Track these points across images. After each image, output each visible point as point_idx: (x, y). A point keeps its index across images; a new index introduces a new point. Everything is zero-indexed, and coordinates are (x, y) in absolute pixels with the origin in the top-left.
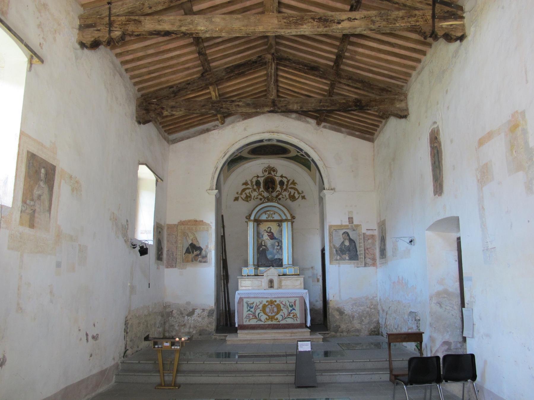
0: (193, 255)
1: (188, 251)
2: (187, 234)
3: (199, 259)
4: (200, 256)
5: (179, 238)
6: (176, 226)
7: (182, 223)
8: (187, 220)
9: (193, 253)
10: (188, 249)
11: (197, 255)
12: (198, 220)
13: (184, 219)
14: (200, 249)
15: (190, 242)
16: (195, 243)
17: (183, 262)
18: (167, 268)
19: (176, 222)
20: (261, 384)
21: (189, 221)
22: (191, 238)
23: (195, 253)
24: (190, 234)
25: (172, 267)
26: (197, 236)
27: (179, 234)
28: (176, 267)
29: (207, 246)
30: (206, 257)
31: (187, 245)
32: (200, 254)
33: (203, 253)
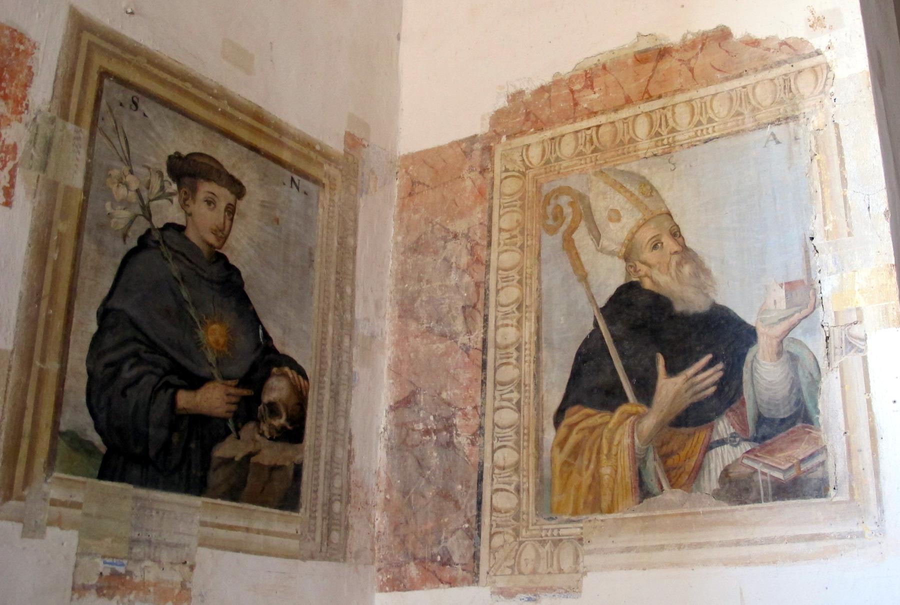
0: (649, 423)
1: (592, 384)
2: (581, 202)
3: (722, 458)
4: (723, 427)
5: (503, 257)
6: (478, 151)
7: (526, 113)
8: (566, 69)
9: (646, 390)
10: (589, 356)
11: (693, 416)
12: (674, 38)
13: (536, 71)
14: (722, 336)
15: (610, 276)
16: (661, 278)
17: (547, 508)
18: (397, 584)
19: (475, 124)
20: (885, 100)
21: (589, 77)
22: (616, 234)
23: (670, 389)
24: (604, 200)
25: (438, 570)
26: (679, 195)
27: (505, 221)
28: (473, 576)
29: (803, 292)
30: (800, 416)
31: (574, 318)
32: (728, 392)
33: (765, 375)
